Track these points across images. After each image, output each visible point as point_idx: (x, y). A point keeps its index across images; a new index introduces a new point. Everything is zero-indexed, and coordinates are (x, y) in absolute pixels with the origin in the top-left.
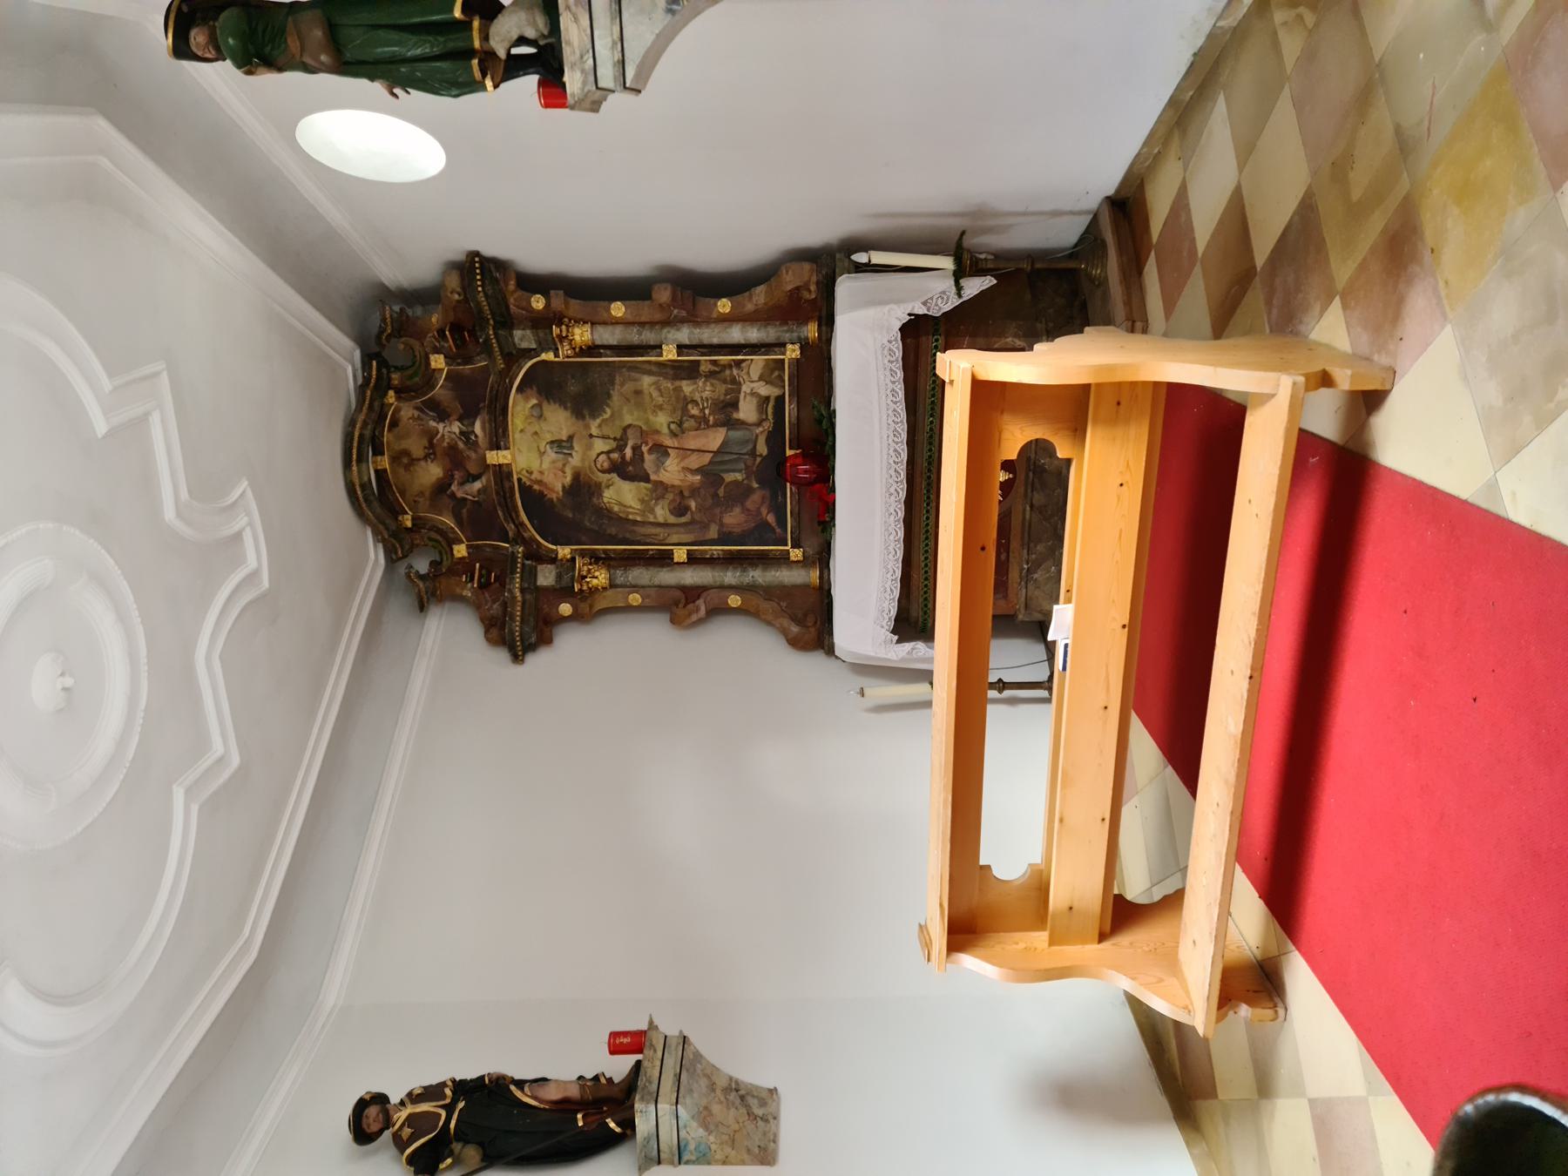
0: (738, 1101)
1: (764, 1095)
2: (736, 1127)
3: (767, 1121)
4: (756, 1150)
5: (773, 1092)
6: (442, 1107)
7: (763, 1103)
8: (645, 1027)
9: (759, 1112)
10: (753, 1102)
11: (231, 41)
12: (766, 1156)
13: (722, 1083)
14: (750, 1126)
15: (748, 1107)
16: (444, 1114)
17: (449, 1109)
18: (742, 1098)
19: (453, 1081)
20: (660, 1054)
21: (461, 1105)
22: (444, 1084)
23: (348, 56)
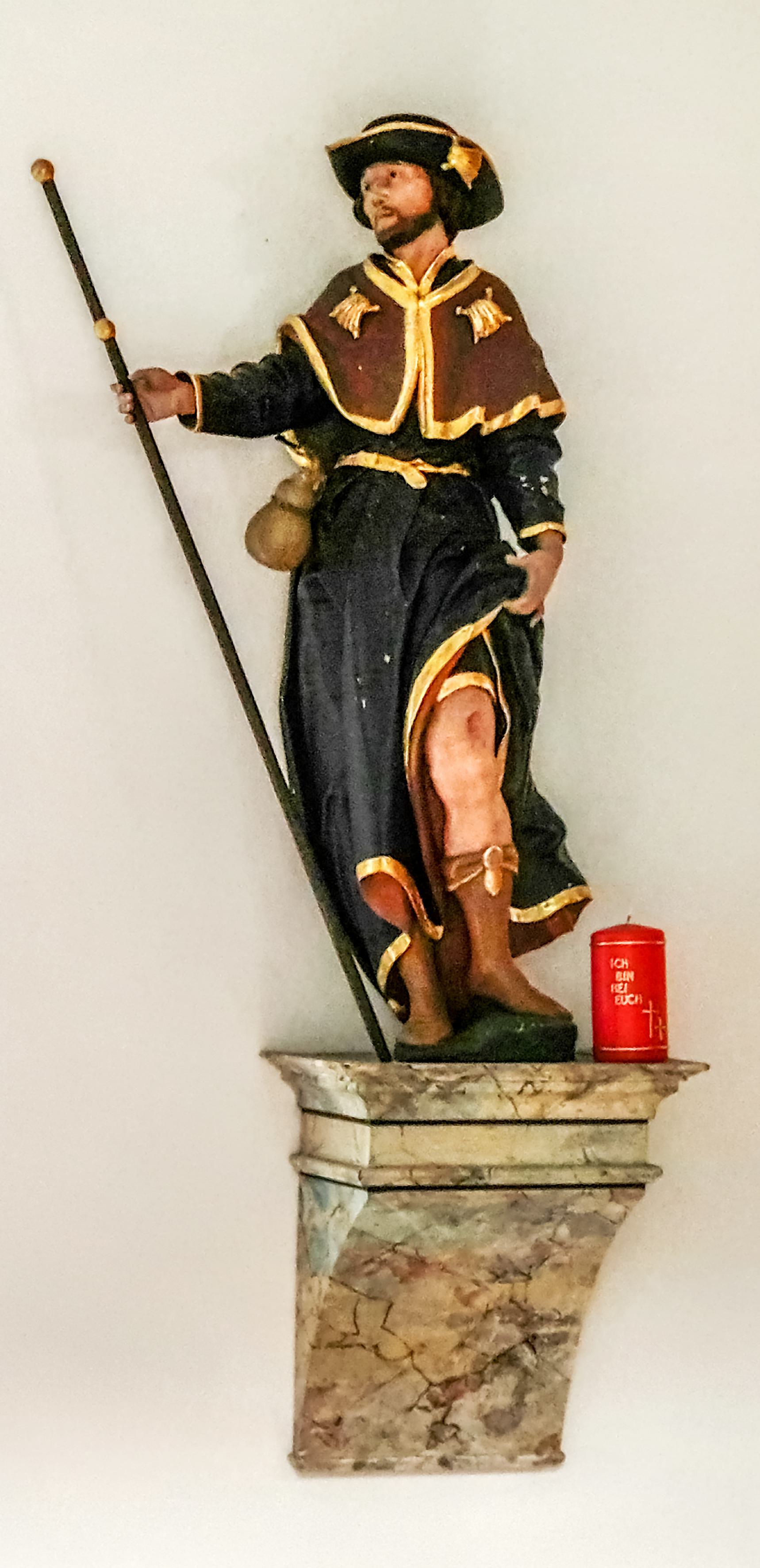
0: (488, 1346)
1: (533, 1425)
2: (394, 1349)
3: (434, 1437)
4: (326, 1414)
5: (549, 1451)
6: (412, 412)
7: (496, 1424)
8: (675, 1050)
9: (466, 1412)
10: (499, 1392)
11: (387, 659)
12: (321, 1441)
13: (544, 1293)
14: (411, 1387)
15: (478, 1378)
16: (386, 427)
17: (407, 440)
18: (507, 1359)
19: (556, 419)
20: (569, 1110)
21: (414, 476)
22: (550, 393)
23: (309, 1106)
